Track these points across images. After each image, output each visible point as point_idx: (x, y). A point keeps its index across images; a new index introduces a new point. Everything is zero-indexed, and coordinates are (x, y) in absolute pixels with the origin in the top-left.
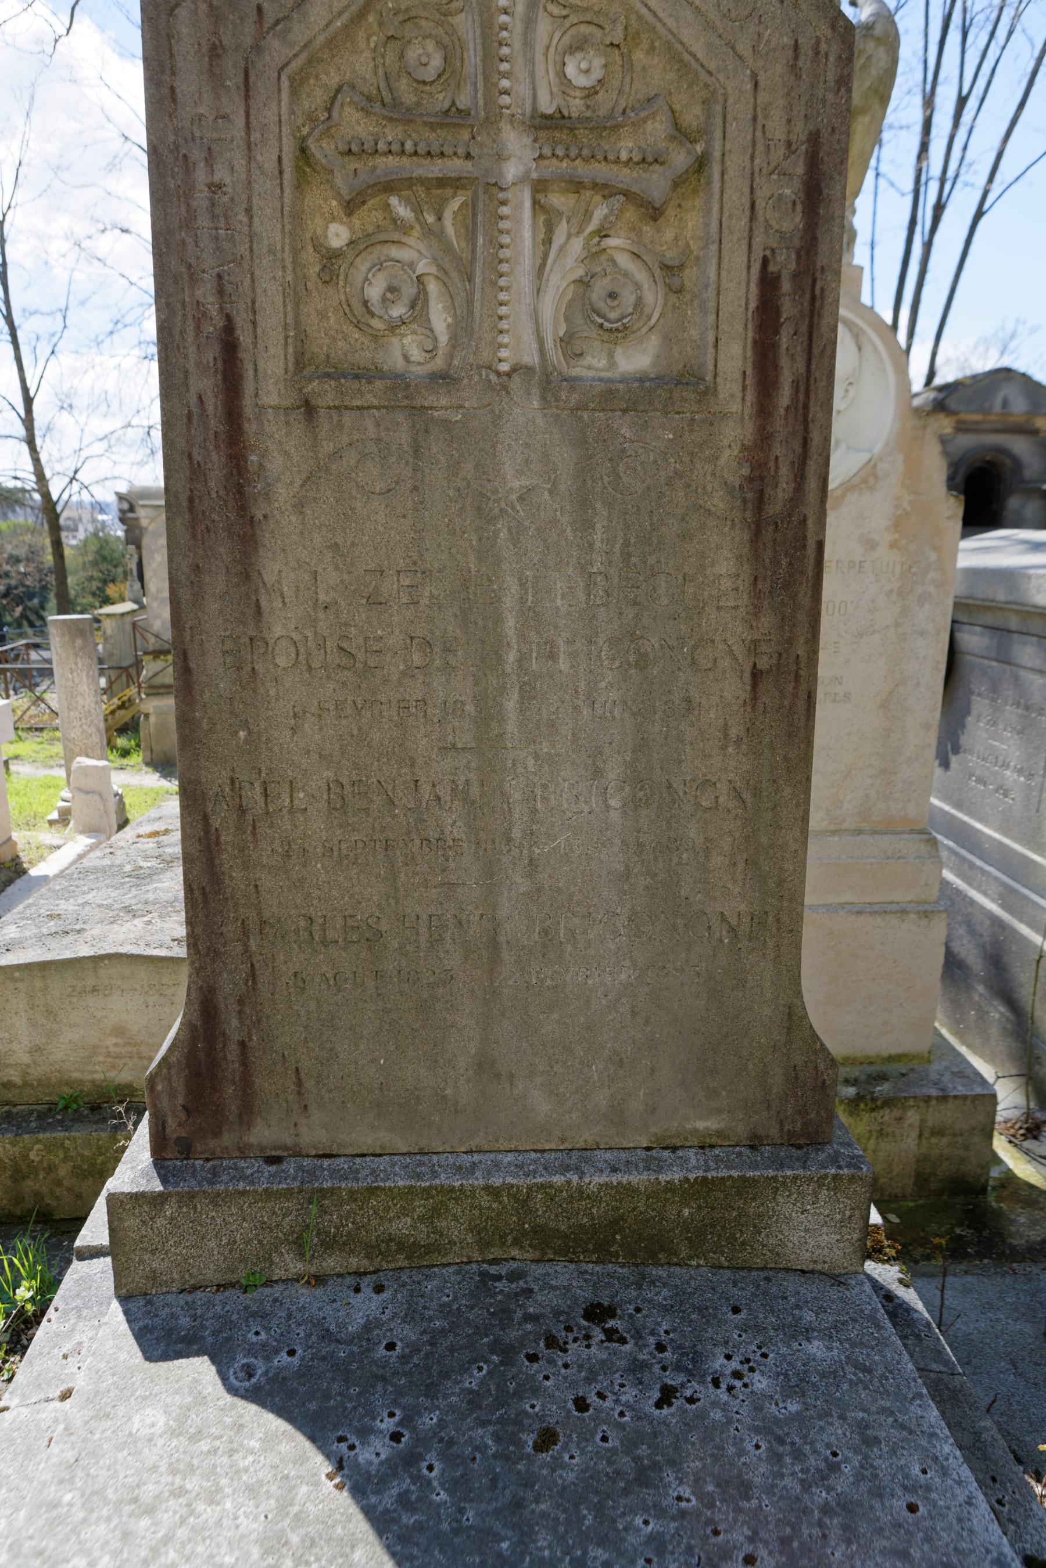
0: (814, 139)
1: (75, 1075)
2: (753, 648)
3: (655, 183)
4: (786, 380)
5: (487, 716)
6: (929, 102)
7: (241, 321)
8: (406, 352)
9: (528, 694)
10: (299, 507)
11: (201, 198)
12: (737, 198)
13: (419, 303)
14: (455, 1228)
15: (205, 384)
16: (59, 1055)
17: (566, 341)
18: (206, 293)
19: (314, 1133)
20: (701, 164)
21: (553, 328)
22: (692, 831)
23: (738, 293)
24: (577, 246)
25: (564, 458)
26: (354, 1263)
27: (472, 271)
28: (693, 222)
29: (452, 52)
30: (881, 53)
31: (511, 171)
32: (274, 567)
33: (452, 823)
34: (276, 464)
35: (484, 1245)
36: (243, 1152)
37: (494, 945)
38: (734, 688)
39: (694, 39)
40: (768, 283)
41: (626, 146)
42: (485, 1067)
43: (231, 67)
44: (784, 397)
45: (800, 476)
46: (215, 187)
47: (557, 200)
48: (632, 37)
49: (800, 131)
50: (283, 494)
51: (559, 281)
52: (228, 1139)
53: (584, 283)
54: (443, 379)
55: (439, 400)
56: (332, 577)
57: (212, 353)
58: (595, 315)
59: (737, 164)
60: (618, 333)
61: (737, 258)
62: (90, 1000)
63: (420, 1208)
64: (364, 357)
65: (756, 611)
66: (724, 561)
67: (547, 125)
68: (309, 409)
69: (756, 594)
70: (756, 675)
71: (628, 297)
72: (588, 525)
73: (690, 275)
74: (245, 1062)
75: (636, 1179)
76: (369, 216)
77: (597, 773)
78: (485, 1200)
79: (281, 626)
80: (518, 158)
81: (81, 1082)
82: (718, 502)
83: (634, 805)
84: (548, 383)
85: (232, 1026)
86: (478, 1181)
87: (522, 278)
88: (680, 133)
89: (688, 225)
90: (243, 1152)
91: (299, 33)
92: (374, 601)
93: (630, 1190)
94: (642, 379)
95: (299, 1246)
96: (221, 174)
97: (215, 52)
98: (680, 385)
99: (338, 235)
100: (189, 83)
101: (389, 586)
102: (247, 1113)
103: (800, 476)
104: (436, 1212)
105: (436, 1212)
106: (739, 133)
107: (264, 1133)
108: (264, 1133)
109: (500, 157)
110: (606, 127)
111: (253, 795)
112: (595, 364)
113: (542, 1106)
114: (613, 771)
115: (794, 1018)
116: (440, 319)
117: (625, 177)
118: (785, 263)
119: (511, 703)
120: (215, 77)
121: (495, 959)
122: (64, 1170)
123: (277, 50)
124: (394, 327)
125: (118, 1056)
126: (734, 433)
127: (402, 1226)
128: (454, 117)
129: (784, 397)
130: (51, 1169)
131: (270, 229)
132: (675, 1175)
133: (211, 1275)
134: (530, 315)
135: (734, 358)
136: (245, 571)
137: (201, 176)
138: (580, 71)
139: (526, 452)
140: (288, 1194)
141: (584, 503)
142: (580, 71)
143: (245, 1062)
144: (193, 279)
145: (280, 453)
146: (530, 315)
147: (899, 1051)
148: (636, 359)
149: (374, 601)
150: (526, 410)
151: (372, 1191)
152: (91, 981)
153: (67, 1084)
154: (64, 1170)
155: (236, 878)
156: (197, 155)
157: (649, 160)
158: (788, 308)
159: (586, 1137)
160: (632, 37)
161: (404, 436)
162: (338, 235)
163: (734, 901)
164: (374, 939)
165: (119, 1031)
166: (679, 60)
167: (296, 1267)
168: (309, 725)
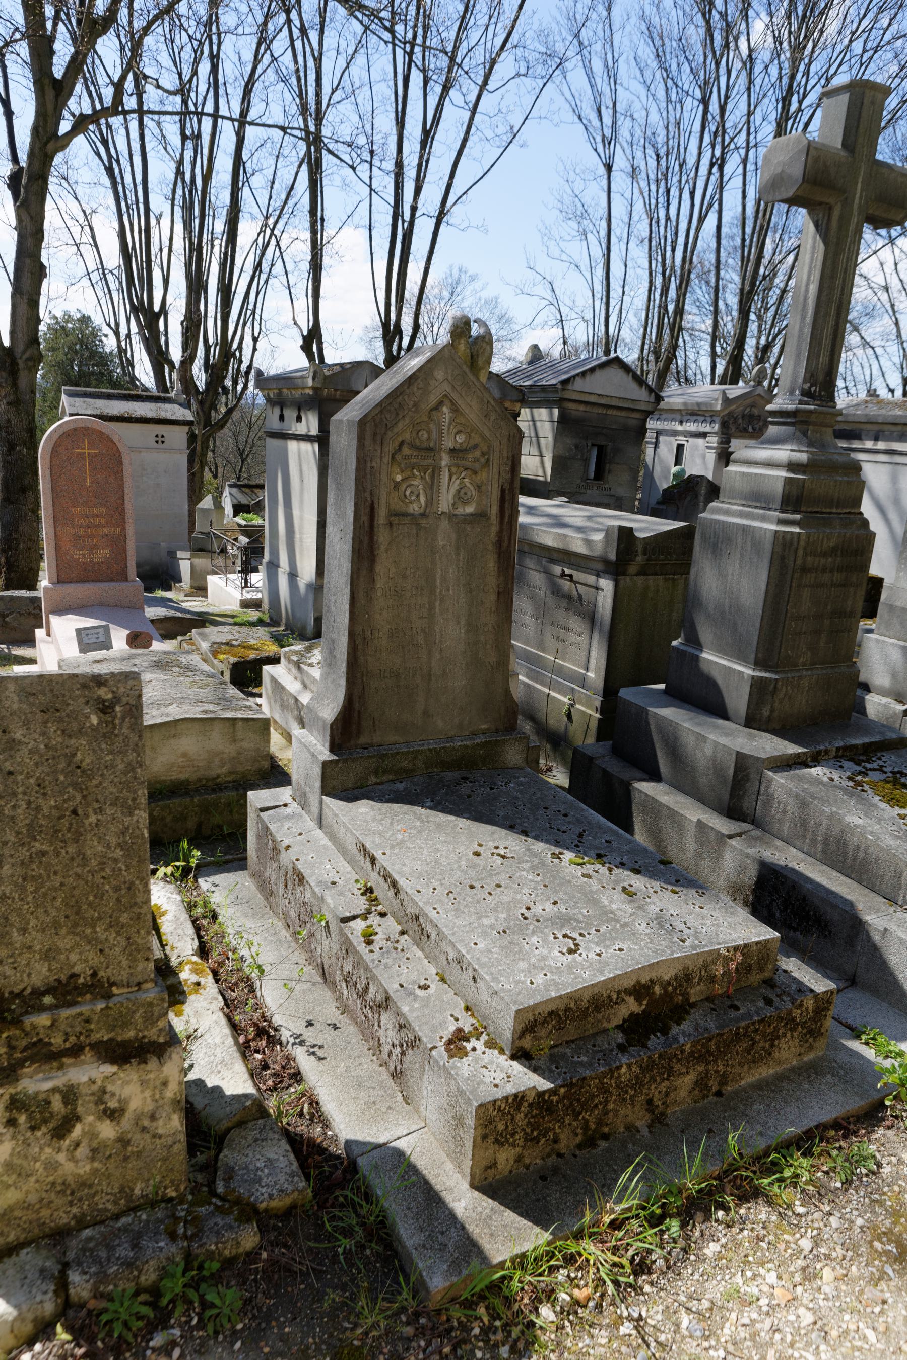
0: (513, 456)
1: (163, 778)
2: (498, 586)
3: (477, 466)
4: (507, 514)
5: (431, 608)
6: (401, 124)
7: (376, 501)
8: (414, 508)
9: (442, 601)
10: (387, 551)
11: (369, 469)
12: (496, 470)
13: (418, 496)
14: (420, 764)
15: (365, 518)
16: (155, 769)
17: (453, 505)
18: (367, 495)
19: (377, 739)
20: (488, 460)
21: (451, 501)
22: (482, 638)
23: (496, 494)
24: (458, 481)
25: (453, 536)
26: (391, 777)
27: (432, 487)
28: (484, 475)
29: (429, 432)
30: (488, 347)
31: (443, 463)
32: (379, 568)
33: (421, 639)
34: (381, 539)
35: (427, 768)
36: (356, 746)
37: (430, 675)
38: (493, 597)
39: (487, 433)
40: (503, 491)
41: (470, 456)
42: (426, 713)
43: (379, 438)
44: (506, 520)
45: (510, 540)
46: (372, 468)
47: (454, 470)
48: (472, 431)
49: (510, 454)
50: (383, 547)
51: (453, 490)
52: (352, 743)
53: (459, 491)
54: (423, 515)
55: (423, 522)
56: (393, 570)
57: (367, 510)
58: (460, 498)
59: (496, 462)
60: (466, 503)
61: (495, 485)
62: (172, 741)
63: (410, 757)
64: (403, 509)
65: (499, 576)
66: (491, 564)
67: (452, 451)
68: (391, 525)
69: (499, 571)
70: (499, 593)
71: (469, 494)
72: (458, 554)
73: (483, 488)
74: (359, 717)
75: (468, 743)
76: (408, 473)
77: (459, 623)
78: (428, 753)
79: (379, 584)
80: (445, 460)
81: (165, 781)
82: (490, 547)
83: (467, 631)
84: (451, 517)
85: (357, 706)
86: (426, 747)
87: (444, 489)
88: (483, 454)
89: (483, 476)
90: (356, 746)
91: (396, 430)
92: (404, 577)
93: (466, 747)
94: (472, 515)
95: (376, 773)
96: (374, 464)
97: (375, 434)
98: (481, 516)
99: (399, 478)
100: (368, 442)
101: (408, 572)
102: (359, 733)
103: (510, 540)
104: (415, 758)
105: (415, 758)
106: (497, 455)
107: (363, 740)
108: (363, 740)
109: (441, 459)
110: (466, 451)
111: (368, 633)
112: (460, 511)
113: (440, 724)
114: (463, 622)
115: (507, 692)
116: (422, 499)
117: (469, 465)
118: (507, 486)
119: (437, 604)
120: (374, 441)
121: (430, 680)
122: (168, 819)
123: (390, 434)
124: (411, 502)
125: (183, 767)
126: (494, 529)
127: (405, 764)
128: (430, 449)
129: (506, 520)
130: (163, 819)
131: (384, 478)
132: (478, 741)
133: (350, 785)
134: (446, 500)
135: (494, 510)
136: (371, 569)
137: (369, 465)
138: (460, 439)
139: (444, 536)
140: (374, 756)
141: (458, 548)
142: (460, 439)
143: (359, 717)
144: (365, 491)
145: (383, 537)
146: (446, 500)
147: (223, 1021)
148: (470, 509)
149: (404, 577)
150: (445, 524)
151: (397, 753)
152: (173, 732)
153: (159, 782)
154: (168, 819)
155: (361, 659)
156: (368, 459)
157: (476, 460)
158: (507, 497)
159: (452, 733)
160: (472, 431)
161: (414, 531)
162: (399, 478)
163: (492, 658)
164: (398, 676)
165: (184, 755)
166: (483, 437)
167: (375, 780)
168: (385, 612)
